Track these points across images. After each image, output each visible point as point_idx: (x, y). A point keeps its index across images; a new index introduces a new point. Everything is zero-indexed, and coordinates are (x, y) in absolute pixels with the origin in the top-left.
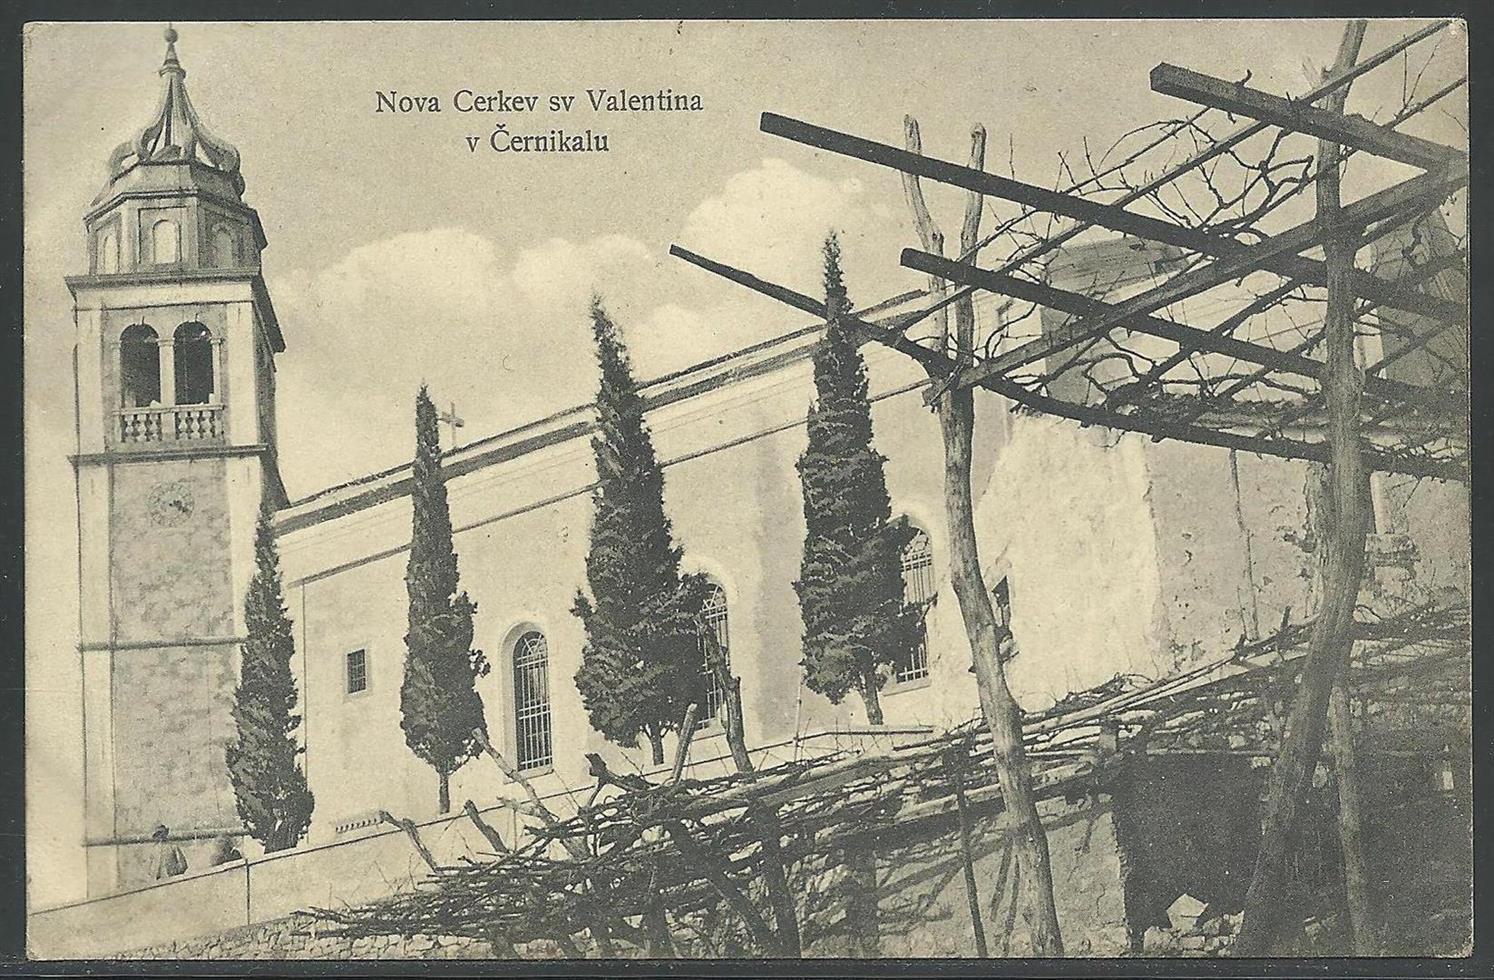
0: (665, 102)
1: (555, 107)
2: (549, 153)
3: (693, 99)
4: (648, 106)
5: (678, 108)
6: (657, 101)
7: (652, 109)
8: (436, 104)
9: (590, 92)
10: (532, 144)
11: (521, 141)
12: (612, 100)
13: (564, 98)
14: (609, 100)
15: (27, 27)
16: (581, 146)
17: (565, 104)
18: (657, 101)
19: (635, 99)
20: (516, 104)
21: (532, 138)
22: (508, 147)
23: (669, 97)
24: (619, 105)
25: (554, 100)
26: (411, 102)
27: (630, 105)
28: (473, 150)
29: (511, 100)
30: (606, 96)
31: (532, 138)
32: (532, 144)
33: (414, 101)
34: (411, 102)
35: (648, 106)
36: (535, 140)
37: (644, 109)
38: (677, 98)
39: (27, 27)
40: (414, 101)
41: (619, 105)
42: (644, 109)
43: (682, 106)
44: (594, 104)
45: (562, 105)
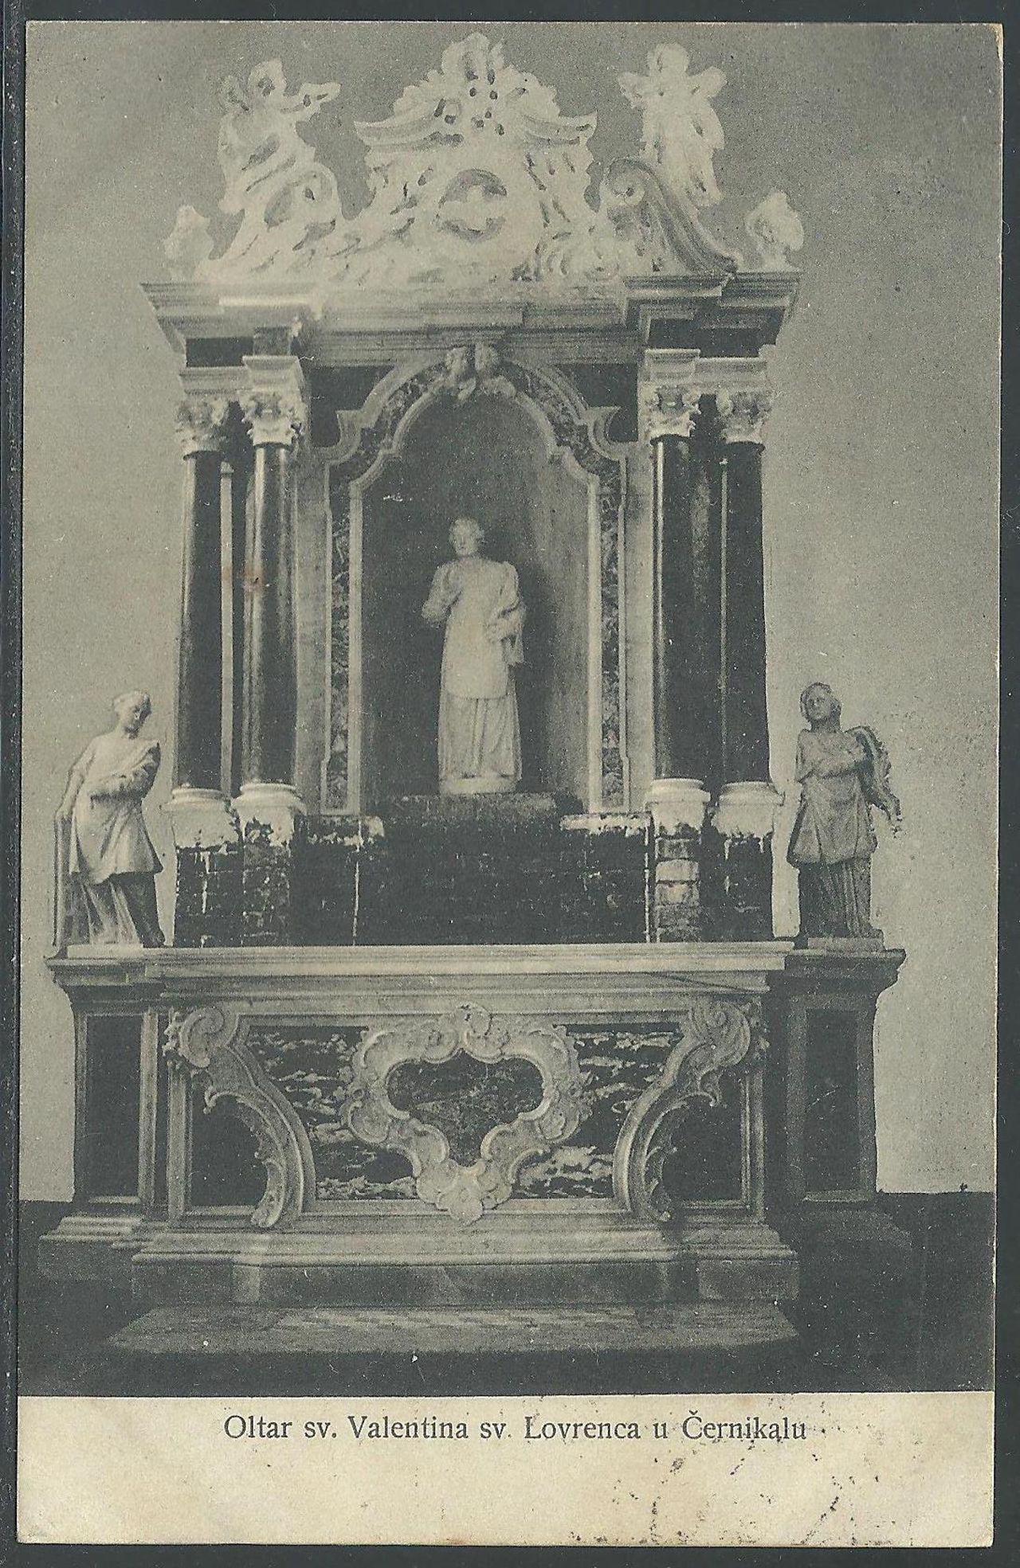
0: (429, 1429)
1: (486, 1434)
2: (438, 1439)
3: (458, 1427)
4: (412, 1433)
5: (443, 1436)
6: (420, 1428)
7: (416, 1436)
8: (636, 1430)
9: (351, 1418)
10: (726, 1430)
11: (714, 1429)
12: (374, 1427)
13: (320, 1424)
14: (371, 1427)
15: (985, 1539)
16: (637, 1434)
17: (322, 1431)
18: (420, 1428)
19: (591, 1426)
20: (395, 1430)
21: (726, 1425)
22: (540, 1436)
23: (434, 1425)
24: (382, 1432)
25: (485, 1427)
26: (554, 1429)
27: (393, 1431)
28: (499, 1437)
29: (583, 1427)
30: (368, 1422)
31: (726, 1425)
32: (726, 1430)
33: (557, 1428)
34: (554, 1429)
35: (412, 1433)
36: (729, 1427)
37: (408, 1436)
38: (442, 1425)
39: (985, 1539)
40: (557, 1428)
41: (382, 1432)
42: (408, 1436)
43: (447, 1434)
44: (355, 1428)
45: (317, 1430)
